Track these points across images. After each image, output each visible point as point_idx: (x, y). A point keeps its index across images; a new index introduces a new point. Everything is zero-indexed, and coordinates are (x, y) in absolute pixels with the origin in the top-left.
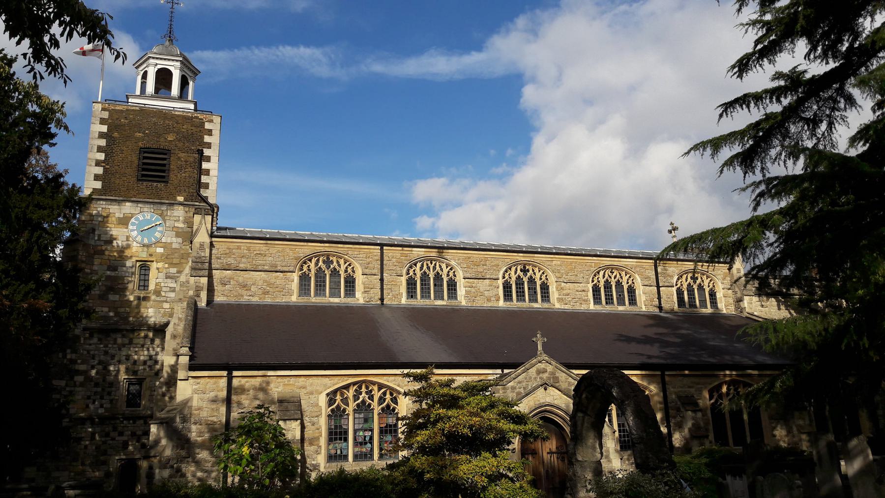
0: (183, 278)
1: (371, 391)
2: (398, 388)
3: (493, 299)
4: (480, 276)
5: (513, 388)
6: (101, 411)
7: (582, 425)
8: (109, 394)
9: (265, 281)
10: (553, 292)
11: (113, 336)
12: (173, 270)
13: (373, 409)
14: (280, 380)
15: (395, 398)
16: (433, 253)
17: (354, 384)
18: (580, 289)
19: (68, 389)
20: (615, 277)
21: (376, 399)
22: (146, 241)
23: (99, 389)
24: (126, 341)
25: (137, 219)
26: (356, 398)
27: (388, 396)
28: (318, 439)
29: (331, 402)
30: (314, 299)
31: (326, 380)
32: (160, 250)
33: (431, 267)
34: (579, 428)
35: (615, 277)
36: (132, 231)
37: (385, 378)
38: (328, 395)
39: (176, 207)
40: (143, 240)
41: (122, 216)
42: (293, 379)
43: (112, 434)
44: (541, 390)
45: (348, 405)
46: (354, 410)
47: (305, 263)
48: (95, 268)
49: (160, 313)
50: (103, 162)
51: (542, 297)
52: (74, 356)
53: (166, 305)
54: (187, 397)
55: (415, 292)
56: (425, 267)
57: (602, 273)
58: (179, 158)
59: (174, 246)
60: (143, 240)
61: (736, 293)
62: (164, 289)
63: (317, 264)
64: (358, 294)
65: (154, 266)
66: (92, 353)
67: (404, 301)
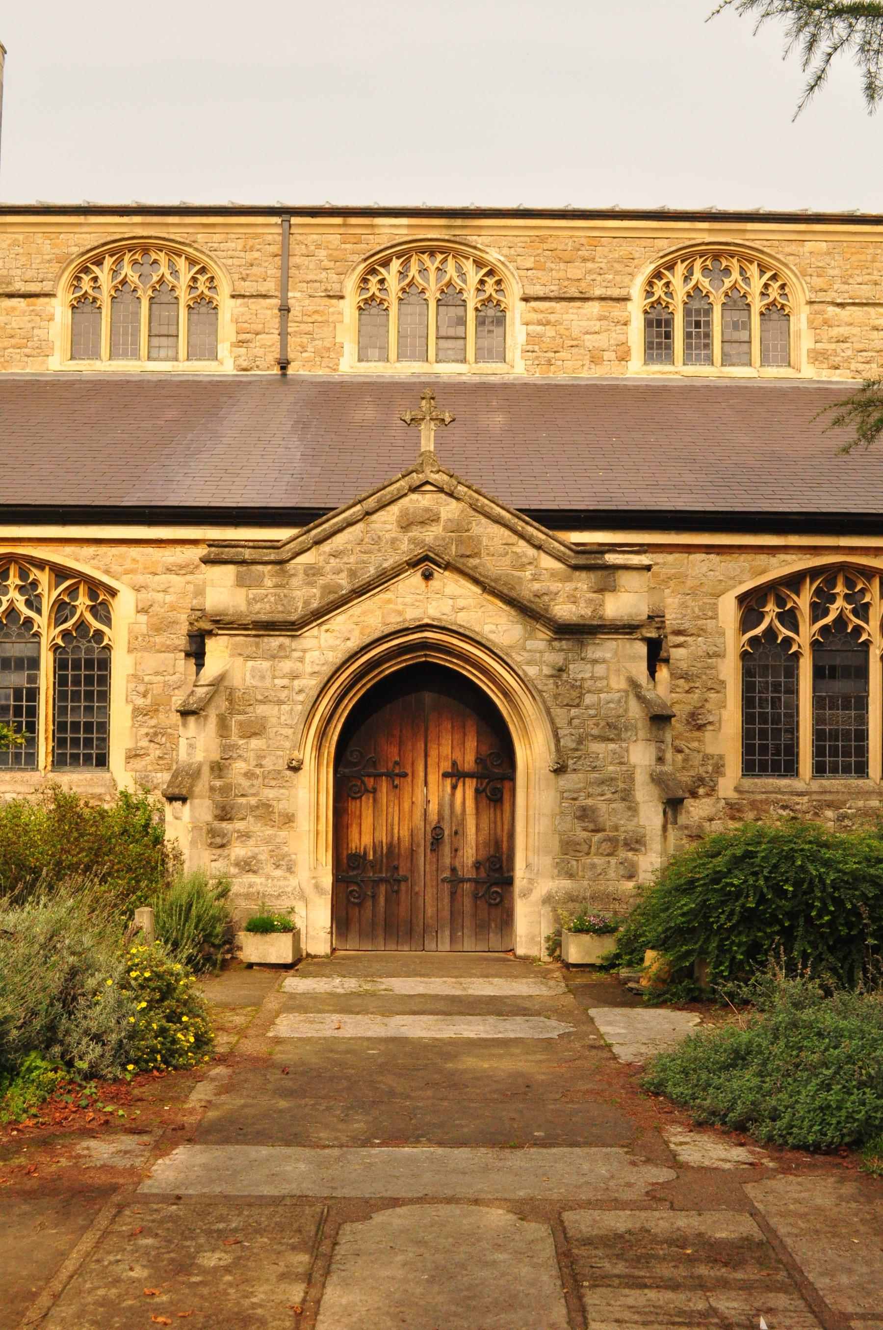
3: (607, 355)
4: (573, 292)
5: (313, 572)
13: (867, 644)
16: (433, 231)
26: (818, 610)
30: (105, 366)
37: (69, 549)
44: (413, 580)
47: (373, 271)
63: (402, 274)
64: (224, 349)
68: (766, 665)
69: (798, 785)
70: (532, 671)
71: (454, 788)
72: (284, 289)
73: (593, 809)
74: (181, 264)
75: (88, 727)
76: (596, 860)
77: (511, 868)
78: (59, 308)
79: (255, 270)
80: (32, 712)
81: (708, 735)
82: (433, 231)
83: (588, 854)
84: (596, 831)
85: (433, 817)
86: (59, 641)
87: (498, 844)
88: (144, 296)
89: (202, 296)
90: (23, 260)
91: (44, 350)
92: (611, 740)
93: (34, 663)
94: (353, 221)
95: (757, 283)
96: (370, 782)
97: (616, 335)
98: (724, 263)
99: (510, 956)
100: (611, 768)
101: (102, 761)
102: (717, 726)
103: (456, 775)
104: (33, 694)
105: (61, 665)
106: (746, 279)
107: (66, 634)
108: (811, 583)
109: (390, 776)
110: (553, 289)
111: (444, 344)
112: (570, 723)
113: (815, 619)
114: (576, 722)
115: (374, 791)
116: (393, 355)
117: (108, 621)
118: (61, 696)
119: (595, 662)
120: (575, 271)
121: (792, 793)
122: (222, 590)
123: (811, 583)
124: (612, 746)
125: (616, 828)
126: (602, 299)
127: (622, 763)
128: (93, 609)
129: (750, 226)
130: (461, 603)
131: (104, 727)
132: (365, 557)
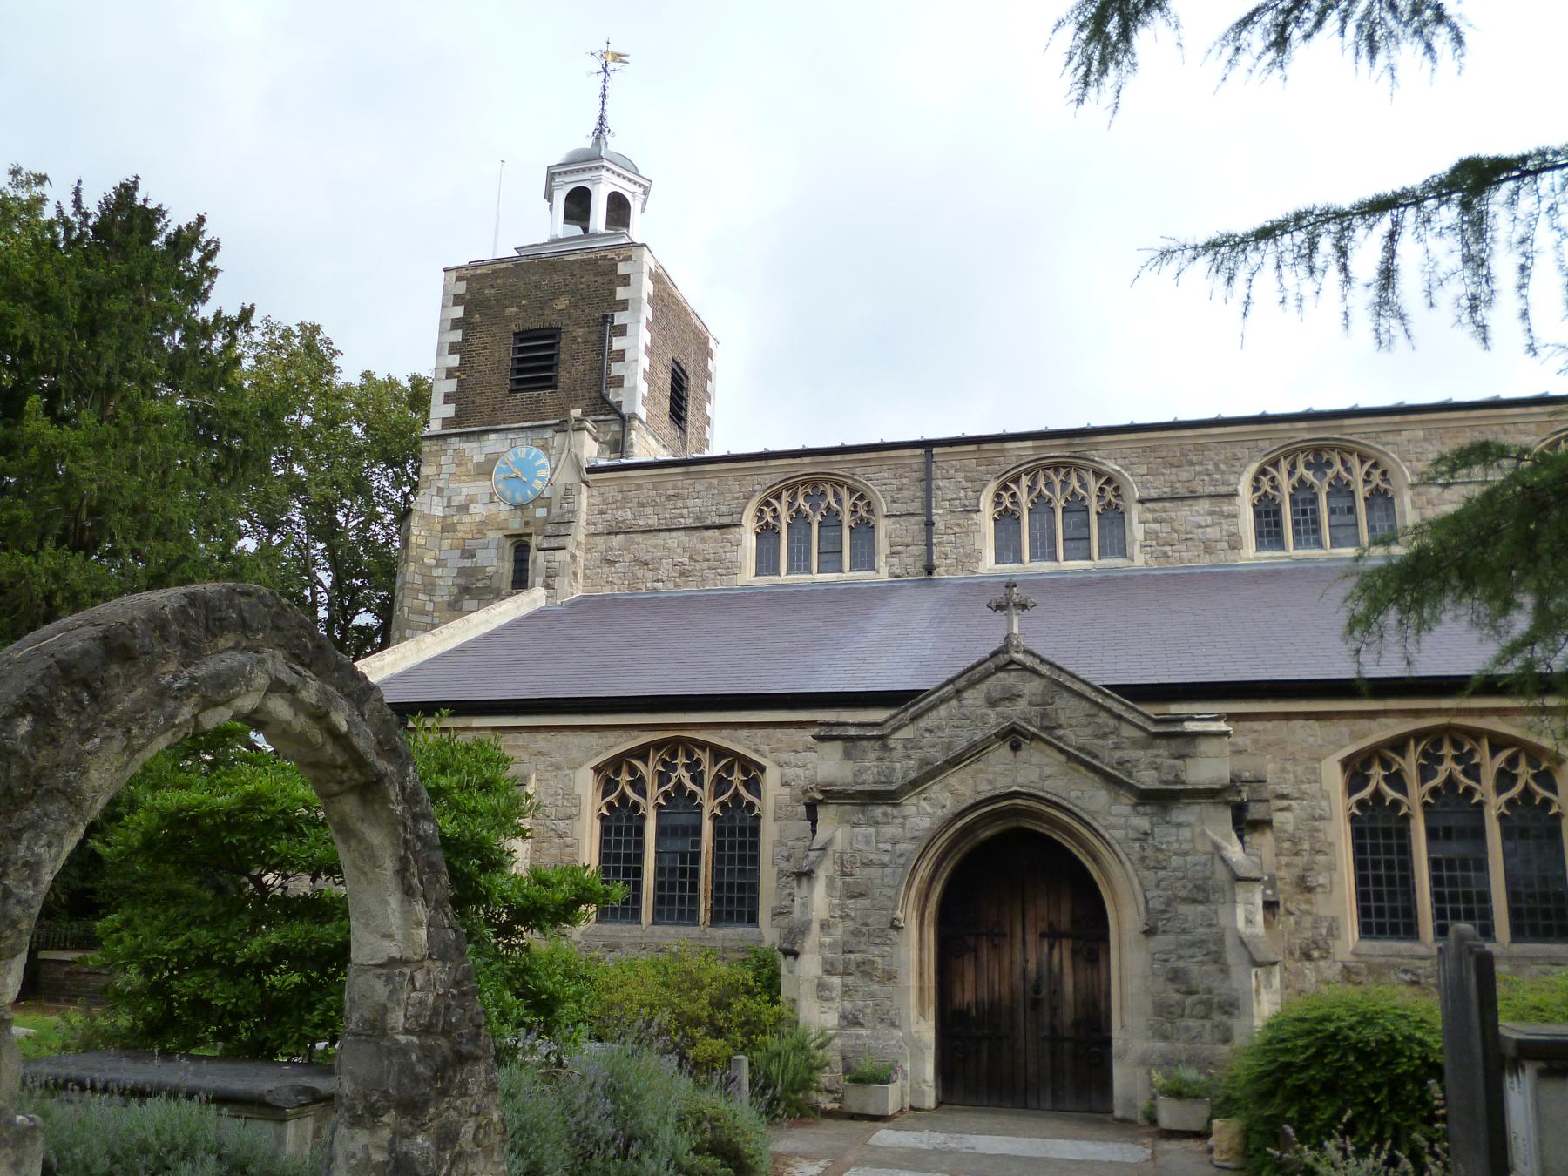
2: (755, 757)
5: (910, 745)
26: (1426, 773)
27: (1524, 771)
29: (608, 786)
30: (784, 578)
31: (593, 739)
37: (726, 732)
44: (1003, 752)
50: (457, 369)
58: (574, 340)
64: (881, 561)
67: (988, 564)
68: (1378, 834)
69: (1419, 949)
71: (1051, 948)
72: (928, 507)
73: (1185, 972)
75: (741, 887)
76: (1191, 1023)
77: (1109, 1029)
79: (905, 493)
80: (695, 873)
81: (1319, 897)
82: (1055, 451)
83: (1182, 1016)
84: (1190, 993)
86: (717, 811)
87: (1095, 1005)
89: (862, 518)
92: (1200, 902)
93: (697, 830)
94: (986, 447)
95: (1359, 472)
96: (971, 941)
98: (1325, 457)
99: (1108, 1117)
100: (1201, 930)
101: (753, 919)
102: (1328, 889)
103: (1052, 935)
104: (696, 857)
105: (718, 832)
106: (1348, 470)
107: (723, 805)
108: (1416, 746)
111: (825, 557)
112: (1158, 885)
113: (1423, 781)
114: (1163, 884)
115: (975, 950)
117: (758, 794)
118: (718, 859)
119: (1179, 825)
121: (1413, 957)
122: (830, 765)
123: (1416, 746)
124: (1200, 908)
125: (1209, 991)
126: (1210, 496)
127: (1210, 925)
128: (746, 784)
129: (1347, 422)
130: (1048, 771)
131: (754, 888)
132: (958, 731)
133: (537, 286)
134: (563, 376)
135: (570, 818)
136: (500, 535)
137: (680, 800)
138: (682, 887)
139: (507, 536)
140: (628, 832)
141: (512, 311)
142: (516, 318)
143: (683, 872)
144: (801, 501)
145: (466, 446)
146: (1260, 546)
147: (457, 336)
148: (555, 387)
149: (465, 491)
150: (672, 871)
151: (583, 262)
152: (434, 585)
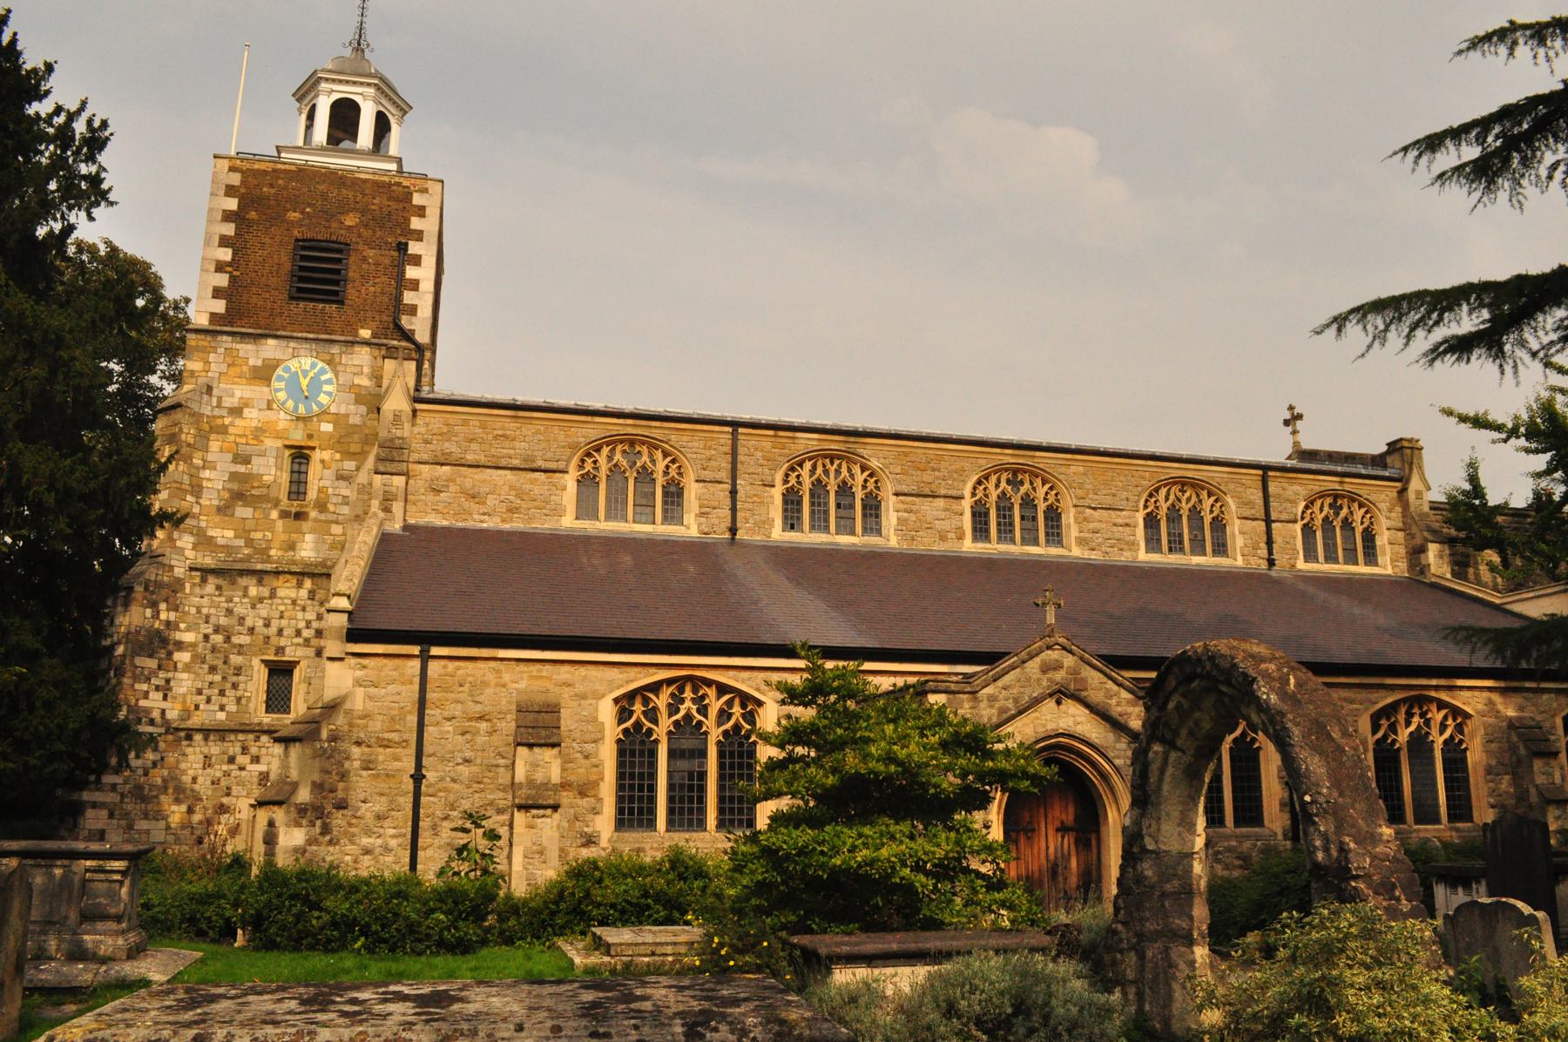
0: (362, 477)
1: (703, 697)
3: (950, 535)
4: (927, 491)
5: (992, 699)
6: (221, 716)
7: (1162, 772)
8: (235, 686)
9: (512, 488)
10: (1069, 526)
11: (243, 581)
12: (350, 465)
13: (706, 733)
14: (522, 667)
15: (751, 713)
16: (835, 444)
17: (670, 682)
18: (1120, 521)
19: (162, 674)
20: (1188, 500)
21: (713, 712)
22: (302, 410)
23: (218, 678)
24: (265, 592)
25: (287, 370)
26: (673, 709)
27: (737, 710)
28: (595, 784)
29: (624, 714)
31: (614, 673)
32: (327, 427)
33: (832, 469)
34: (1153, 779)
35: (1188, 500)
36: (277, 390)
37: (731, 673)
38: (616, 701)
39: (357, 348)
40: (296, 408)
41: (260, 363)
42: (548, 667)
43: (241, 760)
44: (1050, 704)
45: (656, 722)
46: (670, 733)
47: (792, 469)
48: (210, 457)
49: (324, 542)
50: (229, 264)
51: (1047, 534)
52: (172, 616)
53: (336, 529)
54: (343, 692)
55: (799, 519)
56: (819, 470)
57: (1163, 491)
58: (365, 259)
59: (352, 420)
60: (296, 408)
61: (1412, 536)
62: (334, 500)
63: (610, 458)
64: (690, 518)
65: (317, 456)
66: (205, 611)
68: (634, 752)
70: (1117, 762)
74: (659, 455)
78: (570, 481)
79: (713, 463)
82: (835, 444)
85: (1052, 857)
88: (631, 476)
90: (544, 445)
91: (559, 512)
93: (703, 754)
94: (781, 433)
97: (955, 522)
104: (702, 775)
105: (721, 755)
109: (1026, 831)
110: (914, 488)
111: (639, 509)
113: (670, 715)
116: (602, 514)
120: (927, 477)
133: (324, 196)
134: (351, 293)
135: (595, 741)
136: (279, 443)
137: (687, 728)
138: (691, 800)
139: (287, 447)
140: (642, 754)
141: (294, 216)
142: (299, 223)
143: (691, 788)
144: (618, 457)
145: (239, 346)
146: (975, 539)
147: (229, 229)
148: (341, 302)
149: (238, 394)
150: (682, 786)
151: (375, 183)
152: (201, 487)
